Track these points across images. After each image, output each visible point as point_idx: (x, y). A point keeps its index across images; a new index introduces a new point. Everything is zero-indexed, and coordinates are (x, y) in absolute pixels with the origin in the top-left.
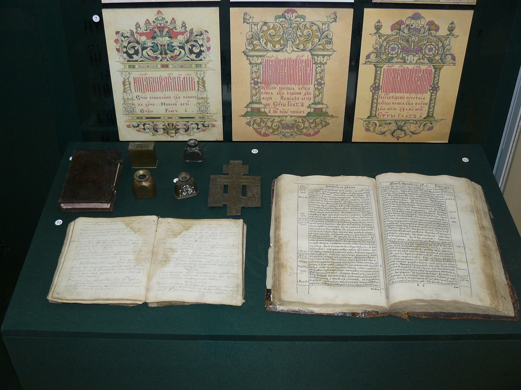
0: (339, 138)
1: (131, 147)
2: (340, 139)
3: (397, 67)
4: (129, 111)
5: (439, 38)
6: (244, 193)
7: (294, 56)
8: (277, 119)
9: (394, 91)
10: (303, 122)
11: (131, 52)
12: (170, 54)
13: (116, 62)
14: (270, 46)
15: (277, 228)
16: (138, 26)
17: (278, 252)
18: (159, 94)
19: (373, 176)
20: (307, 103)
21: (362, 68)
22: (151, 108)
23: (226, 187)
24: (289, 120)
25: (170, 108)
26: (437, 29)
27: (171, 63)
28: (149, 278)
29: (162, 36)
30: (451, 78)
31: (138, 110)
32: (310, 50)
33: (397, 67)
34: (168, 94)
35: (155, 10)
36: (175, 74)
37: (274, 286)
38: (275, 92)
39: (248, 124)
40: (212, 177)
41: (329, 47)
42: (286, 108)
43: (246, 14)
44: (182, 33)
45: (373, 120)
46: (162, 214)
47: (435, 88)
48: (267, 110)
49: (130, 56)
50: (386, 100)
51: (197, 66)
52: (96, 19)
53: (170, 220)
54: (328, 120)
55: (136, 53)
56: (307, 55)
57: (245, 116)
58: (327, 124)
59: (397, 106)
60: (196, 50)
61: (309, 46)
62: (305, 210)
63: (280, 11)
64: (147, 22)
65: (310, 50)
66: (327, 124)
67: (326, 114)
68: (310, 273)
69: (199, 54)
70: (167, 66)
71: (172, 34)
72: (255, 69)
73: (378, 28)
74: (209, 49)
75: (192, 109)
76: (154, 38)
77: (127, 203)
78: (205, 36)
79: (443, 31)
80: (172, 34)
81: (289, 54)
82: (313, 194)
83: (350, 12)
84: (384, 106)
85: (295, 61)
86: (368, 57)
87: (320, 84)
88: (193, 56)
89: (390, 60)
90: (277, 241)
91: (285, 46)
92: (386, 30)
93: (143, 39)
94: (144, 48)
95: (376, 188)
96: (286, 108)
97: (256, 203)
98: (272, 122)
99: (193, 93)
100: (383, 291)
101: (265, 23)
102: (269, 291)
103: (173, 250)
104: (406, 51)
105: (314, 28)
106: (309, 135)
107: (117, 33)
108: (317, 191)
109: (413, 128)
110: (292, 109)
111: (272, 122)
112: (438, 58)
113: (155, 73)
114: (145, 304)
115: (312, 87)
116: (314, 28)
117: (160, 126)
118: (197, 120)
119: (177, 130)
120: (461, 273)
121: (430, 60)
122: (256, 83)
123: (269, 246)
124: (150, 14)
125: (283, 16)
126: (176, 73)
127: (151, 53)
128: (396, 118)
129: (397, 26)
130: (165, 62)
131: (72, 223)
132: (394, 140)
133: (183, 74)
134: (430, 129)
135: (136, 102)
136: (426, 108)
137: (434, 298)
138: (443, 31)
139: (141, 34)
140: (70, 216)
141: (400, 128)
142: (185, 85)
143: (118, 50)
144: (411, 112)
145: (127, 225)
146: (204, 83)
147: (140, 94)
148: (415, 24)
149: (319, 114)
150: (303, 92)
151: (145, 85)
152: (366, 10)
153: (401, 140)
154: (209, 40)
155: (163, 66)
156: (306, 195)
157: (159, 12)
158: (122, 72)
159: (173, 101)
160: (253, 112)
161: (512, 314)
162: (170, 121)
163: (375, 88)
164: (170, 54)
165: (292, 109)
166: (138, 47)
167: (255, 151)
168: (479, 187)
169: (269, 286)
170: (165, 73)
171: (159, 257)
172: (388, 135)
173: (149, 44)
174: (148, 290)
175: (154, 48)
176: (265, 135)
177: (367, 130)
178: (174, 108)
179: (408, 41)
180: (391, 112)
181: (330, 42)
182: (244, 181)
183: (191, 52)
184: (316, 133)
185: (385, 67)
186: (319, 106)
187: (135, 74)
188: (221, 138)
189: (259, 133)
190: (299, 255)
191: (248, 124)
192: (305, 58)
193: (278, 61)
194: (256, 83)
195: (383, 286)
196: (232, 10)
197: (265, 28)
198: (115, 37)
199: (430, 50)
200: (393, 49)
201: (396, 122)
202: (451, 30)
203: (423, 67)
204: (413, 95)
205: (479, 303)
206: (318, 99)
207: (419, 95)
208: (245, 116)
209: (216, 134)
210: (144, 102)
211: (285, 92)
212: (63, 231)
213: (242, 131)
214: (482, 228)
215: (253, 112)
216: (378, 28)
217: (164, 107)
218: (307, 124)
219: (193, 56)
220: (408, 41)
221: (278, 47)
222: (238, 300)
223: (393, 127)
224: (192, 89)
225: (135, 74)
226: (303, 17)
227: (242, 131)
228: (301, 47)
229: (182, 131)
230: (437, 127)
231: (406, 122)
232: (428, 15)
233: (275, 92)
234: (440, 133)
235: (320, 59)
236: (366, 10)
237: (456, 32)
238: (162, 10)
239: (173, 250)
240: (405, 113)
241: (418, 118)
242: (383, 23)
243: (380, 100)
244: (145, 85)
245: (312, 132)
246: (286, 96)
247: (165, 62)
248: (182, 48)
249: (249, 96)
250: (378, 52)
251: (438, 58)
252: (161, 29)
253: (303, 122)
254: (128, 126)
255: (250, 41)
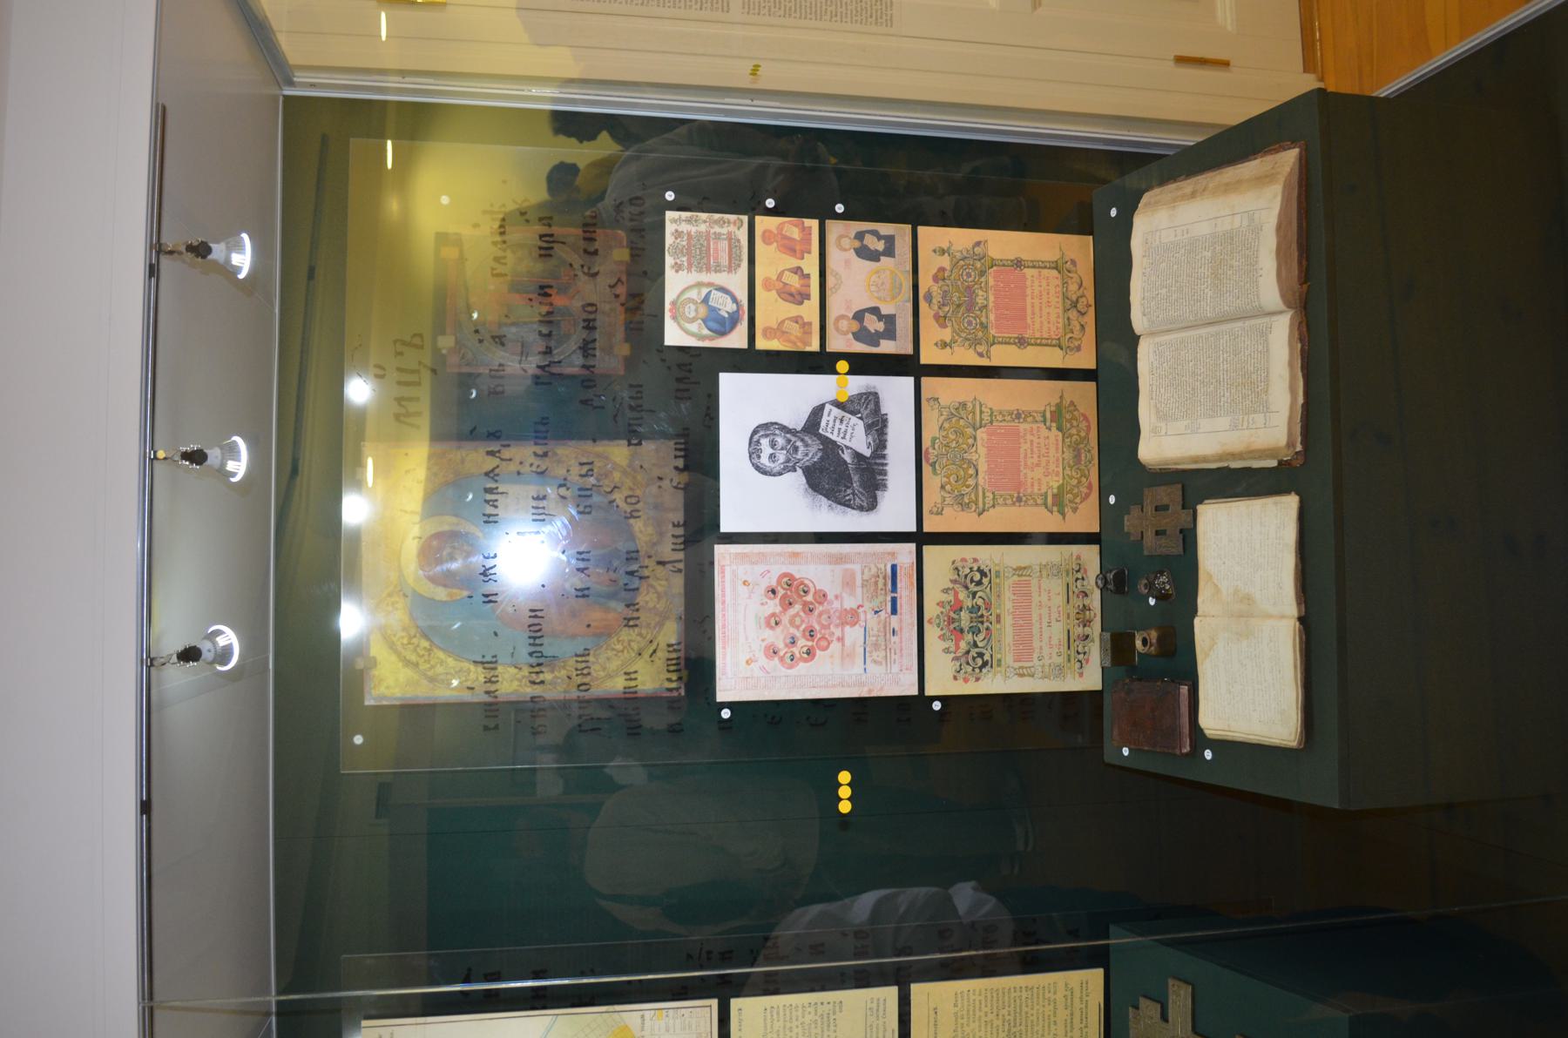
0: (1090, 387)
1: (1108, 664)
2: (1092, 385)
3: (992, 317)
4: (1060, 671)
5: (954, 265)
6: (1166, 508)
7: (982, 451)
8: (1068, 471)
9: (1024, 318)
10: (1071, 436)
11: (980, 662)
12: (983, 611)
13: (993, 684)
14: (971, 482)
15: (1205, 459)
16: (947, 651)
17: (1234, 456)
18: (1036, 630)
19: (1134, 340)
20: (1044, 432)
21: (995, 362)
22: (1055, 641)
23: (1157, 533)
24: (1069, 455)
25: (1055, 616)
26: (942, 269)
27: (995, 611)
28: (1269, 616)
29: (960, 620)
30: (1004, 243)
31: (1059, 660)
32: (975, 429)
33: (992, 317)
34: (1035, 617)
35: (926, 626)
36: (1008, 605)
37: (1272, 457)
38: (1030, 474)
39: (1075, 510)
40: (1146, 553)
41: (970, 405)
42: (1052, 459)
43: (931, 512)
44: (956, 594)
45: (1064, 343)
46: (1194, 611)
47: (1019, 264)
48: (1056, 485)
49: (985, 664)
50: (1037, 326)
51: (998, 576)
52: (937, 706)
53: (1200, 600)
54: (1066, 402)
55: (981, 655)
56: (981, 434)
57: (1063, 514)
58: (1072, 403)
59: (1045, 311)
60: (977, 577)
61: (969, 431)
62: (1181, 425)
63: (926, 468)
64: (942, 637)
65: (975, 429)
66: (1072, 403)
67: (1058, 406)
68: (1255, 412)
69: (983, 574)
70: (998, 616)
71: (958, 608)
72: (1001, 501)
73: (944, 345)
74: (975, 560)
75: (1056, 586)
76: (962, 631)
77: (1176, 663)
78: (959, 564)
79: (945, 262)
80: (958, 608)
81: (981, 456)
82: (1162, 416)
83: (926, 381)
84: (1045, 329)
85: (989, 449)
86: (981, 355)
87: (1018, 416)
88: (985, 581)
89: (984, 327)
90: (1221, 458)
91: (970, 462)
92: (946, 334)
93: (963, 645)
94: (975, 645)
95: (1152, 334)
96: (1052, 459)
97: (1176, 491)
98: (1071, 477)
99: (1034, 582)
100: (1274, 318)
101: (943, 487)
102: (1280, 463)
103: (1236, 591)
104: (971, 306)
105: (946, 425)
106: (1089, 427)
107: (955, 678)
108: (1158, 412)
109: (1073, 287)
110: (1052, 451)
111: (1071, 477)
112: (978, 265)
113: (1006, 632)
114: (1301, 619)
115: (1023, 426)
116: (946, 425)
117: (1080, 630)
118: (1071, 580)
119: (1085, 608)
120: (1245, 223)
121: (982, 273)
122: (1019, 499)
123: (1227, 468)
124: (931, 633)
125: (933, 465)
126: (1007, 604)
127: (981, 636)
128: (1060, 311)
129: (941, 320)
130: (993, 618)
131: (1207, 732)
132: (1092, 311)
133: (1008, 595)
134: (1074, 262)
135: (1047, 661)
136: (1045, 272)
137: (1273, 255)
138: (945, 262)
139: (957, 647)
140: (1199, 738)
141: (1075, 305)
142: (1023, 593)
143: (977, 679)
144: (1052, 291)
145: (1207, 655)
146: (1020, 568)
147: (1035, 656)
148: (937, 299)
149: (1059, 416)
150: (1029, 437)
151: (1024, 647)
152: (923, 361)
153: (1092, 301)
154: (964, 560)
155: (998, 621)
156: (1163, 425)
157: (930, 622)
158: (1007, 677)
159: (1045, 611)
160: (1059, 502)
161: (1297, 150)
162: (1073, 616)
163: (1022, 342)
164: (983, 611)
165: (1052, 451)
166: (973, 652)
167: (1112, 500)
168: (1146, 198)
169: (1274, 463)
170: (1008, 620)
171: (1245, 610)
172: (1084, 320)
173: (969, 637)
174: (1283, 617)
175: (975, 631)
176: (1090, 487)
177: (1079, 349)
178: (1054, 610)
179: (959, 306)
180: (1053, 318)
181: (964, 405)
182: (1149, 509)
183: (979, 583)
184: (1086, 418)
185: (993, 332)
186: (1048, 415)
187: (1009, 659)
188: (1095, 548)
189: (1087, 495)
190: (1234, 427)
191: (1075, 510)
192: (985, 436)
193: (990, 472)
194: (1019, 499)
195: (1267, 319)
196: (926, 530)
197: (948, 487)
198: (961, 681)
199: (969, 275)
200: (970, 323)
201: (1066, 310)
202: (943, 252)
203: (991, 282)
204: (1029, 291)
205: (1279, 198)
206: (1039, 418)
207: (1028, 283)
208: (1063, 514)
209: (1090, 555)
210: (1046, 651)
211: (1030, 461)
212: (1224, 747)
213: (1086, 519)
214: (1193, 195)
215: (1059, 502)
216: (944, 345)
217: (1054, 623)
218: (1074, 431)
219: (985, 581)
220: (959, 306)
221: (971, 471)
222: (1291, 502)
223: (1073, 314)
224: (1028, 584)
225: (1009, 659)
226: (934, 440)
227: (1086, 519)
228: (971, 441)
229: (1087, 601)
230: (1070, 255)
231: (1065, 297)
232: (925, 283)
233: (1030, 474)
234: (1079, 249)
235: (986, 417)
236: (923, 361)
237: (945, 246)
238: (926, 617)
239: (1236, 591)
240: (1054, 300)
241: (1059, 282)
242: (937, 338)
243: (1038, 335)
244: (1024, 647)
245: (1083, 425)
246: (1035, 460)
247: (993, 618)
248: (974, 594)
249: (1035, 509)
250: (974, 342)
251: (978, 265)
252: (951, 621)
253: (1071, 436)
254: (1081, 675)
255: (965, 506)
